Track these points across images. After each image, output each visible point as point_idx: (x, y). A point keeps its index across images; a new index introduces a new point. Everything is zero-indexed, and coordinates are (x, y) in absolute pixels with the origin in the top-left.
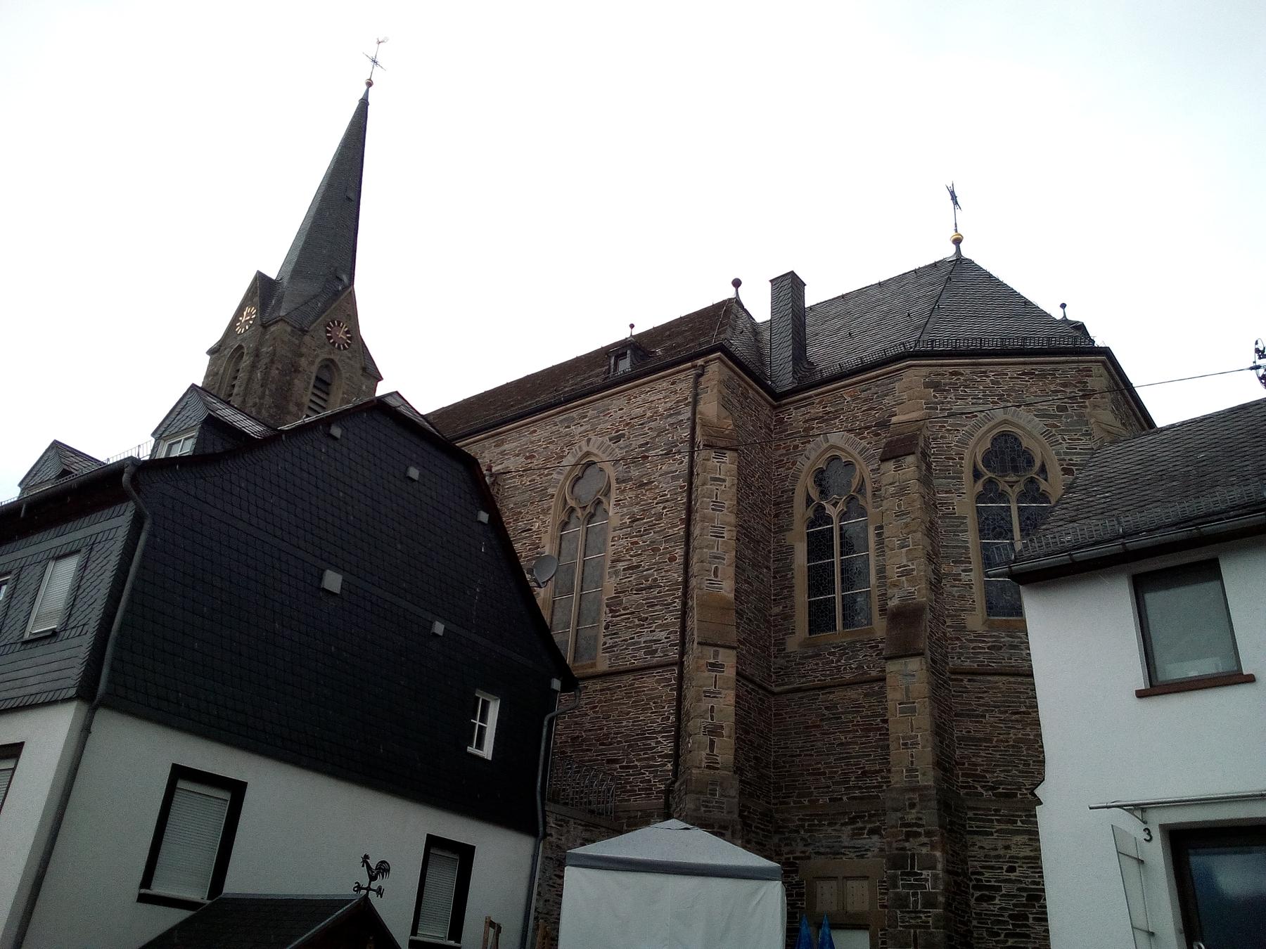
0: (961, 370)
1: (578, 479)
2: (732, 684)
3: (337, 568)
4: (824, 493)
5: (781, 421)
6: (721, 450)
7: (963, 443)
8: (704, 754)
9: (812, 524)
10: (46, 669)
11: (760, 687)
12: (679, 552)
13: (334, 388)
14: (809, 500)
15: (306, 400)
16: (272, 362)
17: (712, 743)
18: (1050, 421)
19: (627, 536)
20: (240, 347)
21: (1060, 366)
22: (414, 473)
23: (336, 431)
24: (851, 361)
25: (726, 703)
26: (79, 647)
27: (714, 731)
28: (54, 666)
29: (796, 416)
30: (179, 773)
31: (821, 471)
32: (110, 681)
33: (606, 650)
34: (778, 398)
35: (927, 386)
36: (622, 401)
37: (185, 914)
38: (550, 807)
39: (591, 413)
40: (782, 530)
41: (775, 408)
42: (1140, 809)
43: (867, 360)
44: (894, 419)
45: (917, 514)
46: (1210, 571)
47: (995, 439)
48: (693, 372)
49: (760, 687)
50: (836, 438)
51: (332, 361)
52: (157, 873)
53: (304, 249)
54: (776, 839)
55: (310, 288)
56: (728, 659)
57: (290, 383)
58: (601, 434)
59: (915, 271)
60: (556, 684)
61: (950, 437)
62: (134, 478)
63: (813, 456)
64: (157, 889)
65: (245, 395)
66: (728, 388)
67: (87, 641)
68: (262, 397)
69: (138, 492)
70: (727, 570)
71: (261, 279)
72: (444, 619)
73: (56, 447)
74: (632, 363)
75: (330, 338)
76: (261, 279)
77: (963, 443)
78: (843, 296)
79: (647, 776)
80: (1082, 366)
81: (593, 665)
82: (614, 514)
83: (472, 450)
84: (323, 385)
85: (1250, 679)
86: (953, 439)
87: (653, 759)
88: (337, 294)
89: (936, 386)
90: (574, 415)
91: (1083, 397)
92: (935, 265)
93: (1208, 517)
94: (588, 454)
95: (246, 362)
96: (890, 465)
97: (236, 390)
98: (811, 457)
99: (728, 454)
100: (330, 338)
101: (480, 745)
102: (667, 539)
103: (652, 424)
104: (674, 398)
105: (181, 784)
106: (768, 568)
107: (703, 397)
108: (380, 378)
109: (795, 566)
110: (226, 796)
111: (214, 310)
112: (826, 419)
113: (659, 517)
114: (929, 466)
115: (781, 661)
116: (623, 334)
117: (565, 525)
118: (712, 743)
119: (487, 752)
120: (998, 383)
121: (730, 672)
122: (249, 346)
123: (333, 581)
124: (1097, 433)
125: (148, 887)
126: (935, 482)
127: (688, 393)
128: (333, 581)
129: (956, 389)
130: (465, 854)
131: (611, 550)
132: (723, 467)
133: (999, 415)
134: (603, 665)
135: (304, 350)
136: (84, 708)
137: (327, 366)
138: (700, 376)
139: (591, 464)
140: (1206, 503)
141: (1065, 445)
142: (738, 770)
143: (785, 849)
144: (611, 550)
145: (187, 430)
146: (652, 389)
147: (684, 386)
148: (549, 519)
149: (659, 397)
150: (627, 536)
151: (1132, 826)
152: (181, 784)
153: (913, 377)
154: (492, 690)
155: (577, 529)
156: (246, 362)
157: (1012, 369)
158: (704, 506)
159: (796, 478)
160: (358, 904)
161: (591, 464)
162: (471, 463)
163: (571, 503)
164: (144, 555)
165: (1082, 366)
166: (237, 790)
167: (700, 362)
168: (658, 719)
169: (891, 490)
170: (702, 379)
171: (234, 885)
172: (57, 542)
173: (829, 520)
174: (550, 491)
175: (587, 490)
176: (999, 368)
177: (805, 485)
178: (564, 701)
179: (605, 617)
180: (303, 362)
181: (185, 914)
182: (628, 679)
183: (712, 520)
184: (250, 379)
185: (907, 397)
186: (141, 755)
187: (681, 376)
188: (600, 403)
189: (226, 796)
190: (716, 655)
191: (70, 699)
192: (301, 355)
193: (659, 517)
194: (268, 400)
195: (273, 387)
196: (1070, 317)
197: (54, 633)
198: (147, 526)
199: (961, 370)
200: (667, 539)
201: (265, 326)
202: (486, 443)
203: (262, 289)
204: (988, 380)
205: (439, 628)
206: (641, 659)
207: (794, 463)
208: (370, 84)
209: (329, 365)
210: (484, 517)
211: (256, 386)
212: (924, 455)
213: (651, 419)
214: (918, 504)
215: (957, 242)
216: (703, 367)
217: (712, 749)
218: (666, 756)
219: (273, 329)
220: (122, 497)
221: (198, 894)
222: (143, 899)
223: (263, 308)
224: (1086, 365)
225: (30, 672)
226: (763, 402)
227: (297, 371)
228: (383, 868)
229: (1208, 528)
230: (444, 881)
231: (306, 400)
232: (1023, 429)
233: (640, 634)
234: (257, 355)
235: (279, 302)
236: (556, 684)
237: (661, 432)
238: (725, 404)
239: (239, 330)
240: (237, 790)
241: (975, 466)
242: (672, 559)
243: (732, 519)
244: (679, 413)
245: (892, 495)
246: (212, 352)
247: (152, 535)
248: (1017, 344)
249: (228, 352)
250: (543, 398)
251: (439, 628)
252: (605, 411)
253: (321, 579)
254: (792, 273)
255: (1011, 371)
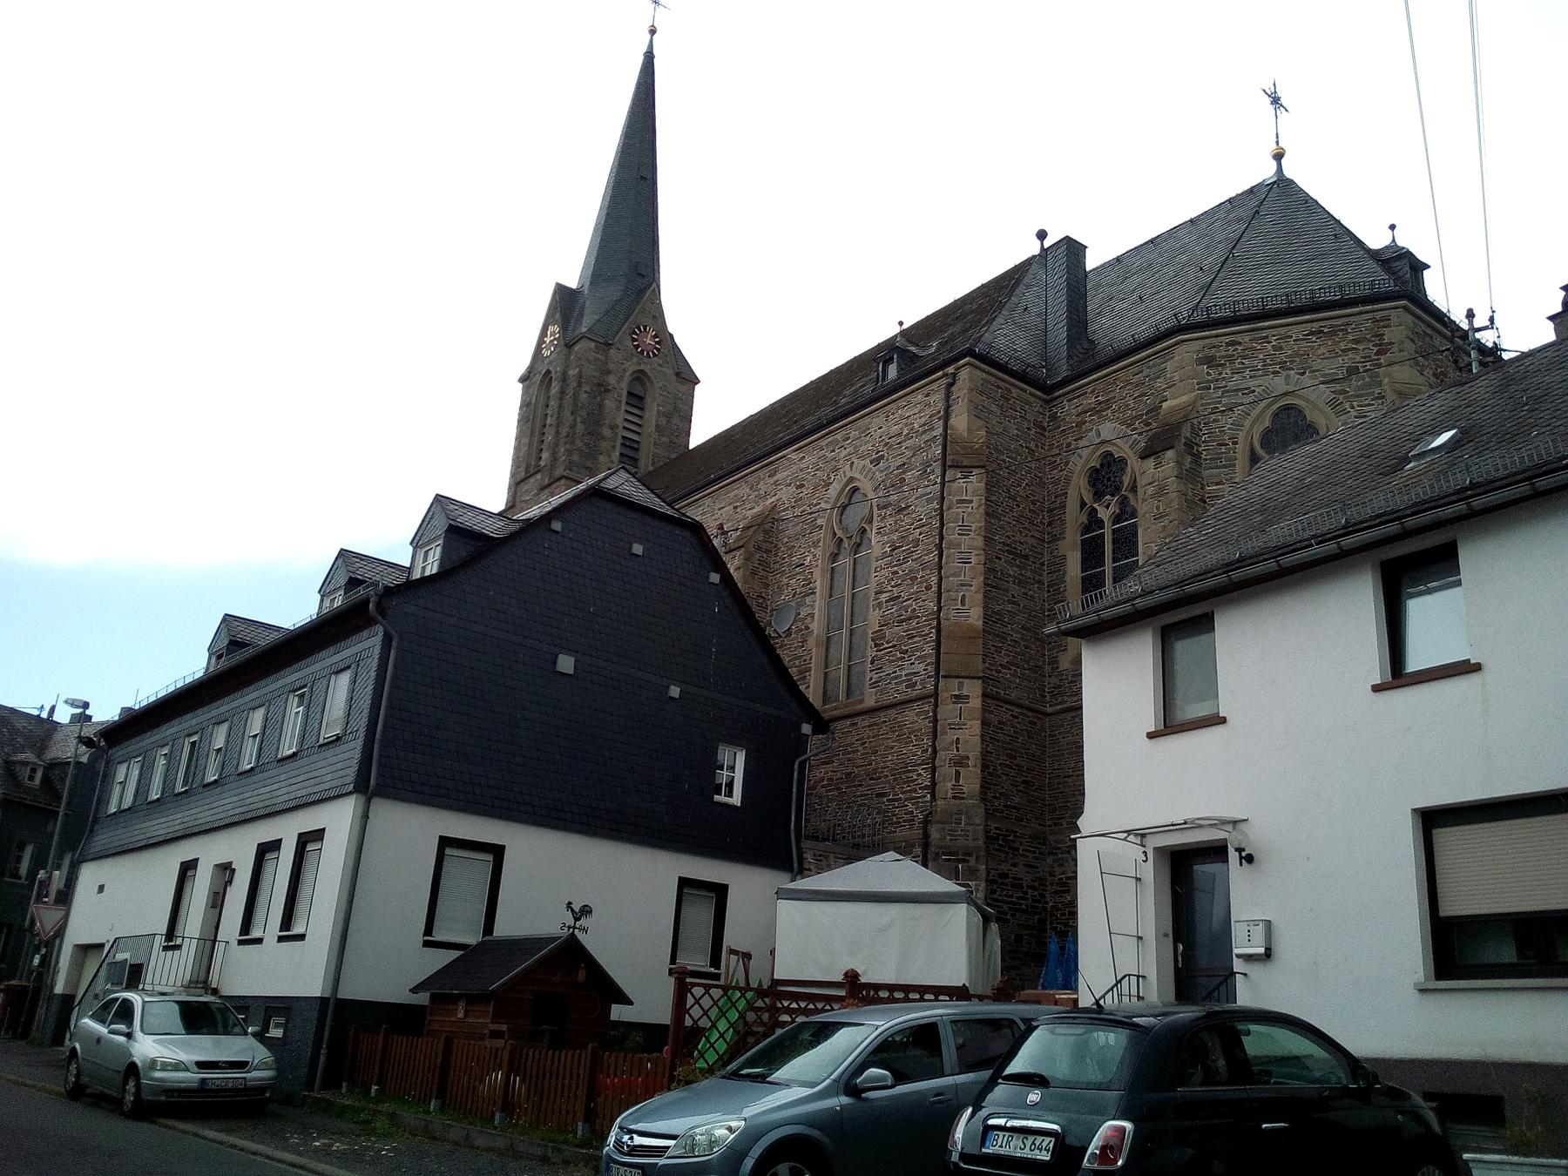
0: (1238, 338)
1: (844, 507)
2: (978, 714)
3: (568, 651)
4: (1098, 496)
5: (1054, 417)
6: (966, 469)
7: (1238, 425)
8: (949, 785)
9: (1086, 529)
10: (334, 768)
11: (1029, 709)
12: (934, 579)
13: (648, 399)
14: (1083, 504)
15: (619, 421)
16: (580, 385)
17: (958, 773)
18: (1338, 387)
19: (889, 565)
20: (548, 372)
21: (1353, 319)
22: (638, 549)
23: (557, 526)
24: (1144, 330)
25: (971, 733)
26: (353, 751)
27: (960, 762)
28: (339, 766)
29: (1068, 409)
30: (445, 842)
31: (1096, 471)
32: (379, 774)
33: (874, 685)
34: (1048, 390)
35: (1200, 362)
36: (878, 419)
37: (457, 954)
38: (806, 844)
39: (854, 434)
40: (1055, 539)
41: (1047, 402)
42: (1142, 835)
43: (1142, 337)
44: (1165, 405)
45: (1174, 515)
46: (1205, 624)
47: (1276, 415)
48: (944, 381)
49: (1029, 709)
50: (1108, 429)
51: (642, 371)
52: (436, 924)
53: (601, 248)
54: (1049, 860)
55: (614, 291)
56: (973, 689)
57: (601, 406)
58: (862, 457)
59: (1229, 201)
60: (806, 729)
61: (1222, 420)
62: (379, 605)
63: (1085, 453)
64: (438, 936)
65: (558, 425)
66: (982, 393)
67: (360, 743)
68: (573, 426)
69: (383, 615)
70: (975, 596)
71: (562, 293)
72: (676, 682)
73: (343, 554)
74: (900, 369)
75: (637, 347)
76: (562, 293)
77: (1238, 425)
78: (1152, 241)
79: (910, 807)
80: (1378, 315)
81: (862, 701)
82: (877, 544)
83: (695, 513)
84: (636, 400)
85: (1223, 721)
86: (1226, 422)
87: (915, 791)
88: (642, 291)
89: (1209, 361)
90: (838, 437)
91: (1378, 353)
92: (1251, 191)
93: (1241, 562)
94: (852, 479)
95: (555, 389)
96: (1151, 462)
97: (549, 421)
98: (1083, 460)
99: (975, 471)
100: (637, 347)
101: (730, 794)
102: (924, 566)
103: (909, 443)
104: (928, 412)
105: (448, 851)
106: (1040, 582)
107: (955, 408)
108: (697, 381)
109: (1067, 578)
110: (490, 857)
111: (517, 334)
112: (1098, 411)
113: (916, 543)
114: (1197, 456)
115: (1054, 680)
116: (889, 331)
117: (834, 557)
118: (958, 773)
119: (736, 799)
120: (1281, 348)
121: (976, 702)
122: (557, 370)
123: (566, 663)
124: (1390, 396)
125: (491, 933)
126: (1205, 473)
127: (941, 405)
128: (566, 663)
129: (1232, 362)
130: (719, 892)
131: (873, 581)
132: (970, 487)
133: (1279, 384)
134: (870, 702)
135: (611, 366)
136: (362, 799)
137: (637, 379)
138: (951, 385)
139: (856, 489)
140: (1191, 566)
141: (1353, 413)
142: (983, 798)
143: (1058, 870)
144: (873, 581)
145: (435, 540)
146: (909, 403)
147: (937, 398)
148: (819, 552)
149: (913, 412)
150: (889, 565)
151: (1133, 851)
152: (448, 851)
153: (1186, 352)
154: (734, 741)
155: (845, 561)
156: (555, 389)
157: (1296, 328)
158: (952, 535)
159: (1068, 481)
160: (566, 940)
161: (856, 489)
162: (697, 529)
163: (839, 534)
164: (395, 666)
165: (1378, 315)
166: (498, 852)
167: (950, 370)
168: (915, 752)
169: (1151, 490)
170: (954, 388)
171: (500, 930)
172: (336, 658)
173: (1100, 524)
174: (819, 522)
175: (854, 516)
176: (1283, 331)
177: (1078, 487)
178: (815, 743)
179: (871, 652)
180: (612, 379)
181: (457, 954)
182: (892, 712)
183: (958, 545)
184: (560, 406)
185: (1178, 382)
186: (413, 831)
187: (934, 386)
188: (861, 423)
189: (490, 857)
190: (961, 685)
191: (350, 793)
192: (609, 372)
193: (916, 543)
194: (580, 428)
195: (584, 413)
196: (1400, 243)
197: (338, 738)
198: (394, 644)
199: (1238, 338)
200: (924, 566)
201: (569, 346)
202: (761, 473)
203: (565, 303)
204: (1269, 346)
205: (675, 691)
206: (897, 692)
207: (1067, 464)
208: (653, 32)
209: (640, 377)
210: (715, 578)
211: (567, 414)
212: (1190, 445)
213: (908, 437)
214: (1175, 505)
215: (1278, 157)
216: (954, 375)
217: (957, 780)
218: (926, 787)
219: (576, 348)
220: (369, 622)
221: (472, 939)
222: (427, 944)
223: (564, 329)
224: (1385, 313)
225: (324, 771)
226: (1032, 399)
227: (607, 391)
228: (586, 911)
229: (1236, 575)
230: (700, 914)
231: (619, 421)
232: (1308, 401)
233: (901, 668)
234: (564, 378)
235: (581, 314)
236: (806, 729)
237: (916, 450)
238: (977, 412)
239: (546, 353)
240: (498, 852)
241: (1252, 450)
242: (928, 588)
243: (980, 542)
244: (932, 429)
245: (1152, 497)
246: (523, 380)
247: (400, 650)
248: (1305, 299)
249: (538, 378)
250: (827, 411)
251: (675, 691)
252: (866, 431)
253: (555, 663)
254: (1067, 239)
255: (1296, 332)
